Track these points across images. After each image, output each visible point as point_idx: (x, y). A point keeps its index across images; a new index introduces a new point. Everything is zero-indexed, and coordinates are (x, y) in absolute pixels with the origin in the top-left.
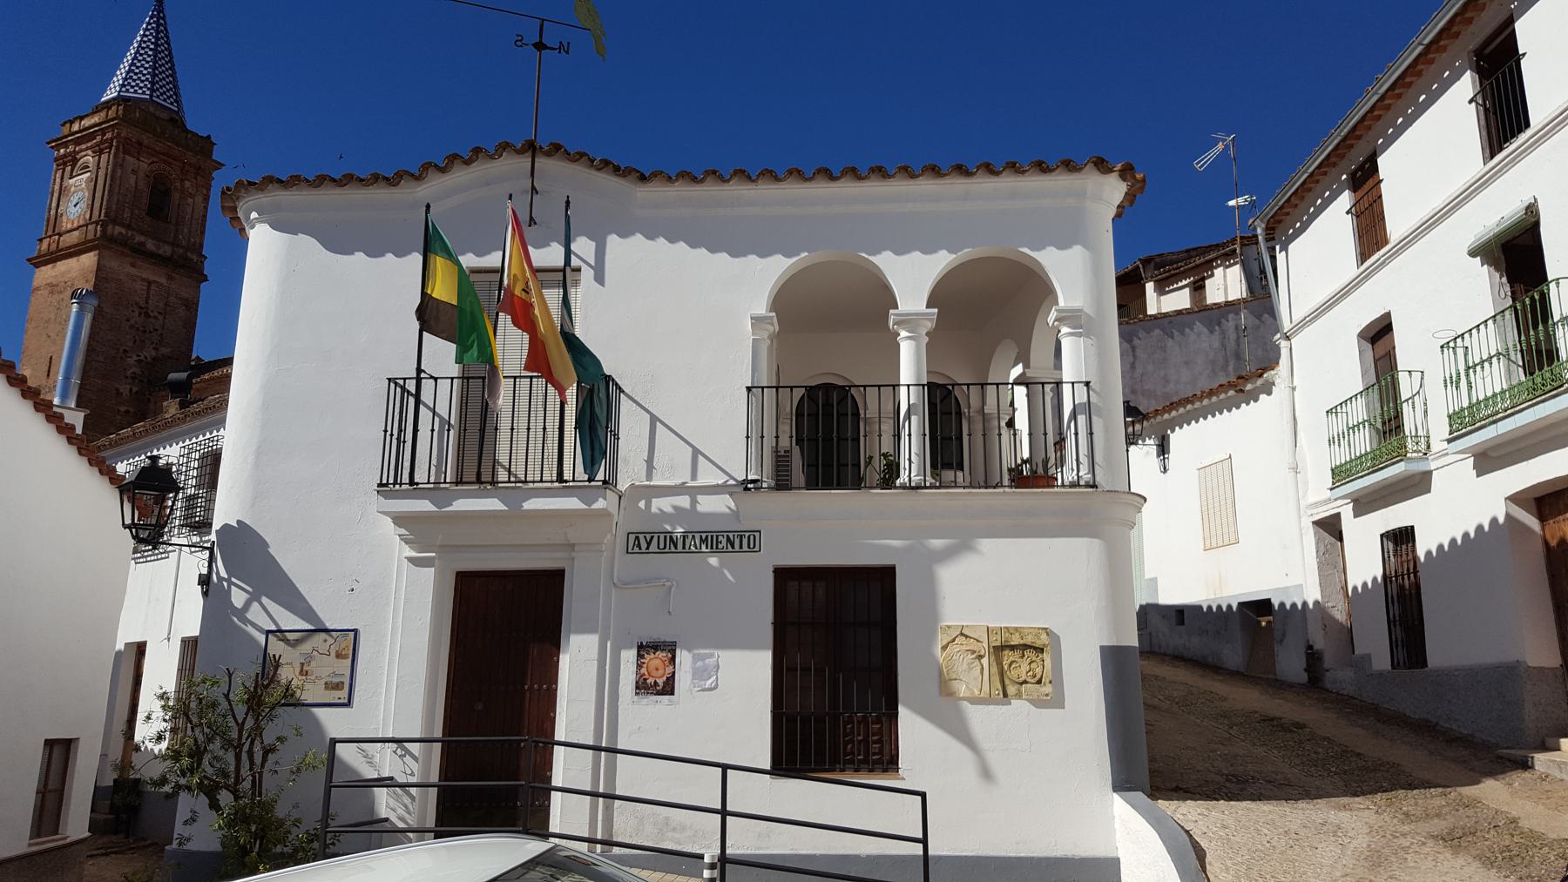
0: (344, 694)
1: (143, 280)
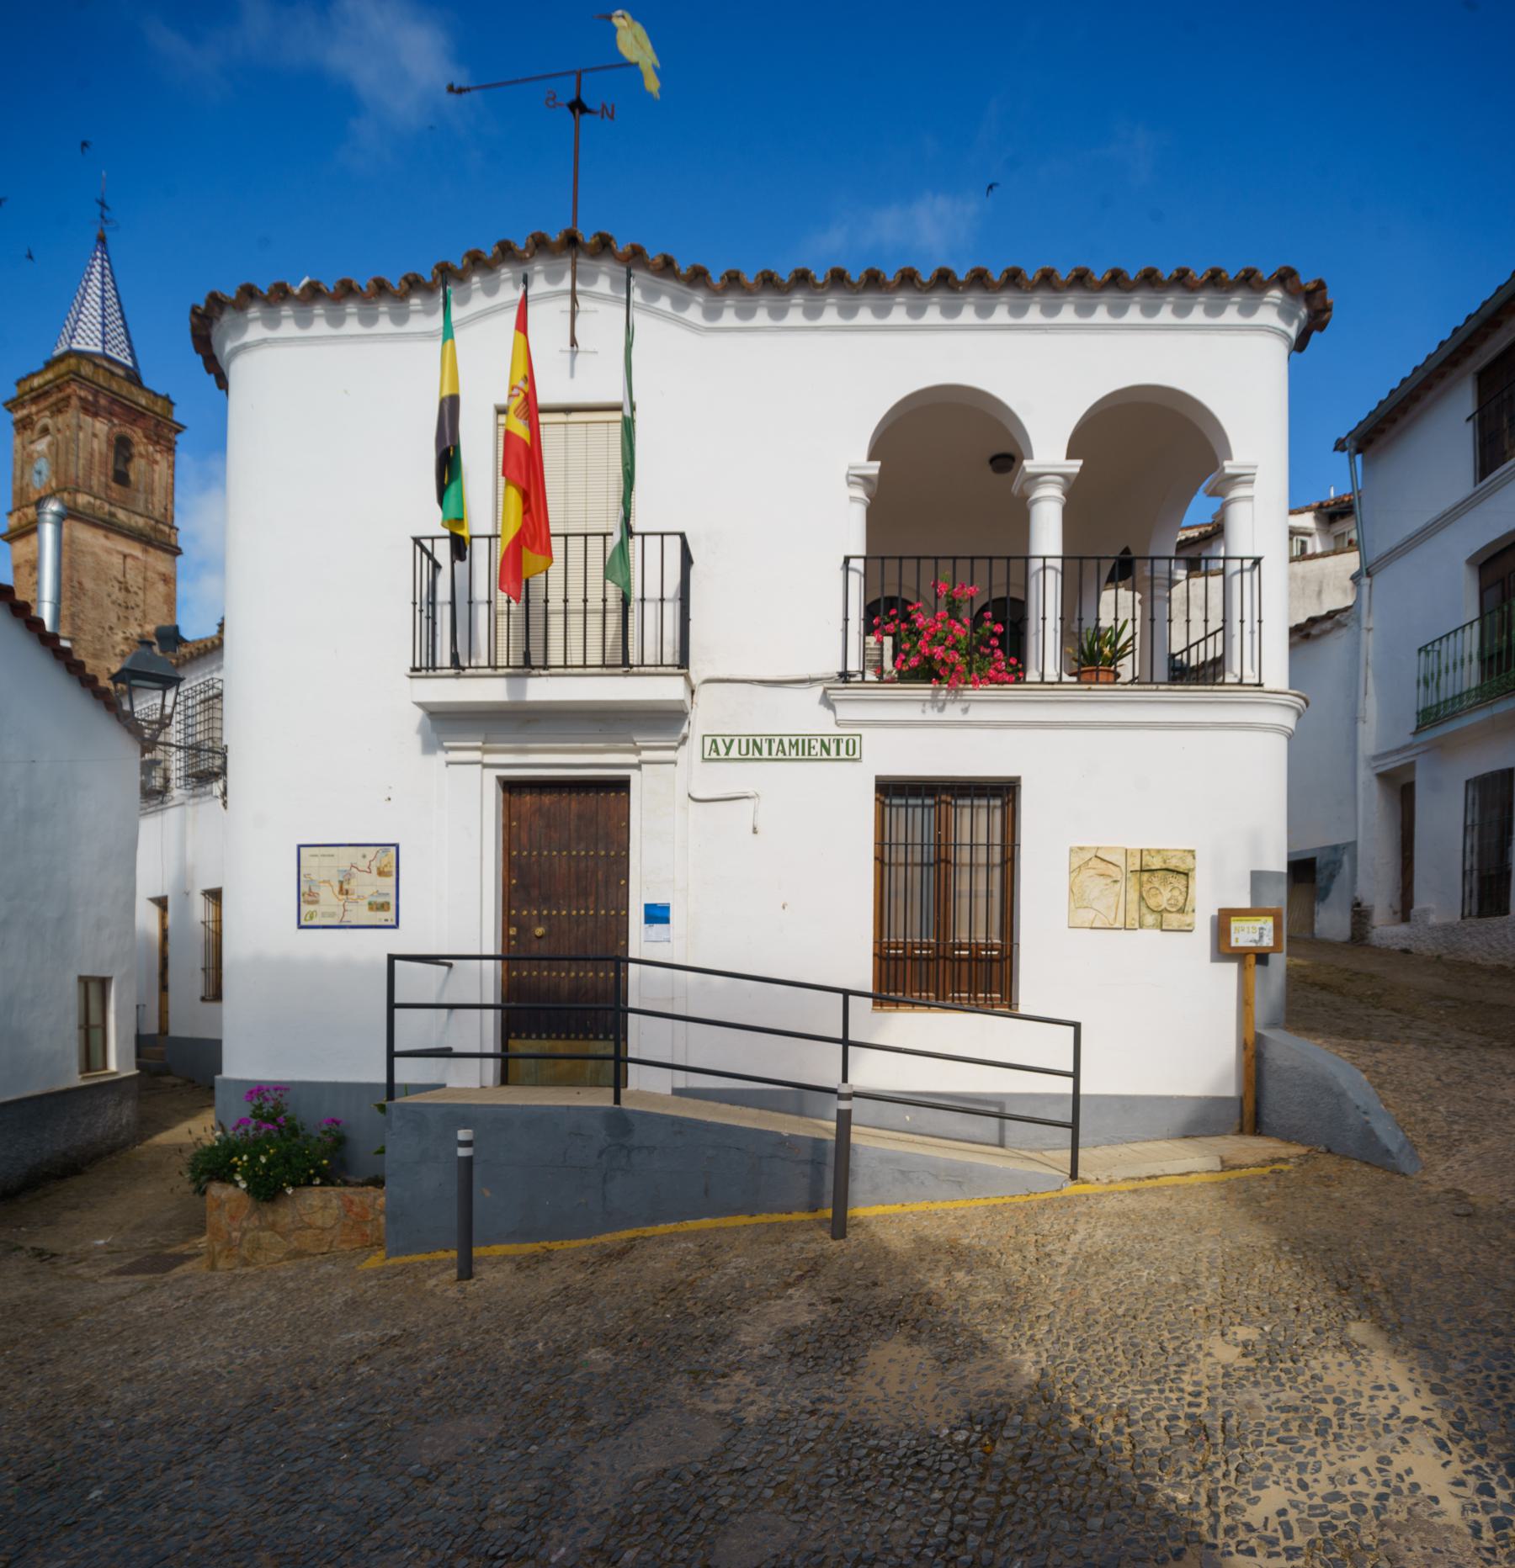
0: (391, 915)
1: (119, 552)
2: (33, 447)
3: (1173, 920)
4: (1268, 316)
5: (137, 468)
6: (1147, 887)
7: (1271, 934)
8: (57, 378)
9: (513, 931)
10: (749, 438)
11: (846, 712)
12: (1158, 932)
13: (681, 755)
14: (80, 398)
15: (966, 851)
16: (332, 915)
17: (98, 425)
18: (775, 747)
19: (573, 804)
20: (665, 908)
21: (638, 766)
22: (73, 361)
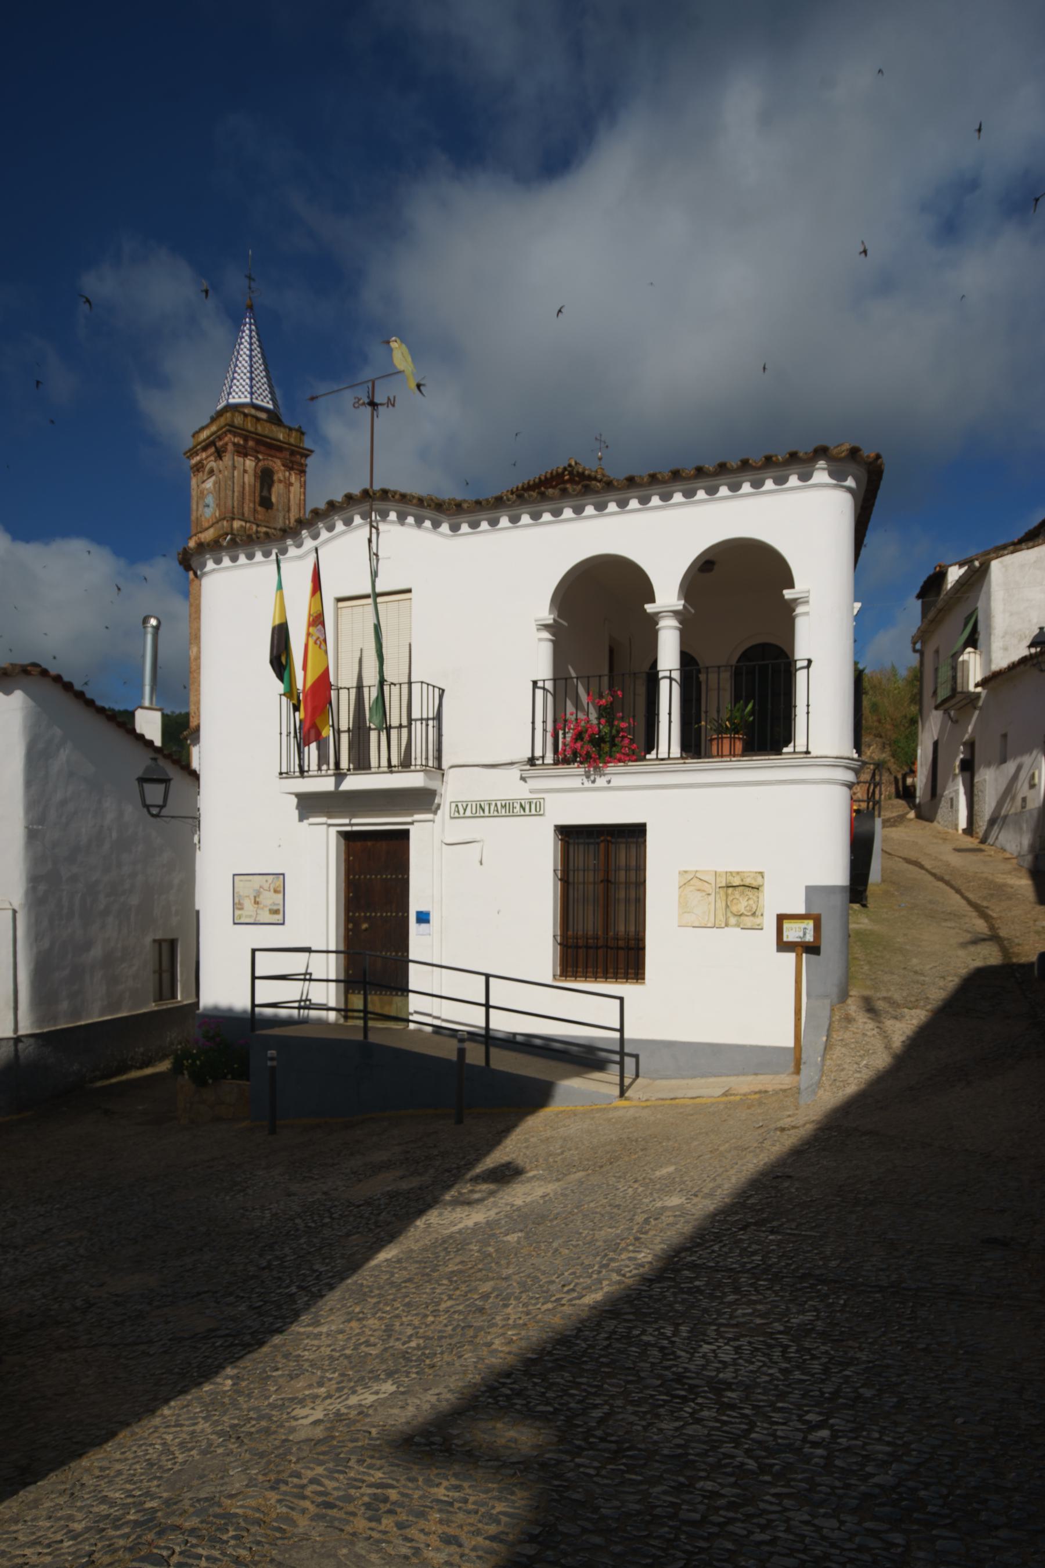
2: (203, 485)
3: (748, 921)
4: (821, 476)
5: (277, 493)
6: (730, 898)
7: (812, 933)
8: (218, 431)
9: (351, 926)
10: (469, 612)
11: (533, 784)
12: (739, 929)
13: (438, 817)
14: (234, 444)
15: (622, 873)
16: (250, 916)
17: (248, 462)
18: (492, 808)
19: (383, 845)
20: (427, 914)
21: (412, 823)
22: (229, 415)
